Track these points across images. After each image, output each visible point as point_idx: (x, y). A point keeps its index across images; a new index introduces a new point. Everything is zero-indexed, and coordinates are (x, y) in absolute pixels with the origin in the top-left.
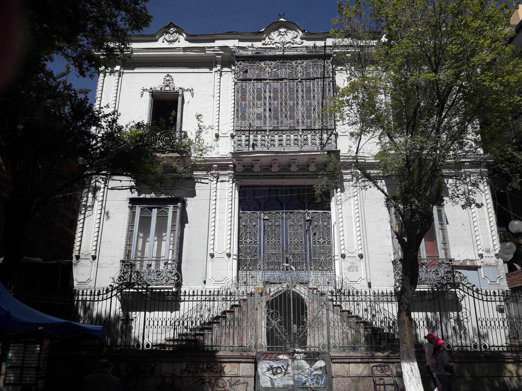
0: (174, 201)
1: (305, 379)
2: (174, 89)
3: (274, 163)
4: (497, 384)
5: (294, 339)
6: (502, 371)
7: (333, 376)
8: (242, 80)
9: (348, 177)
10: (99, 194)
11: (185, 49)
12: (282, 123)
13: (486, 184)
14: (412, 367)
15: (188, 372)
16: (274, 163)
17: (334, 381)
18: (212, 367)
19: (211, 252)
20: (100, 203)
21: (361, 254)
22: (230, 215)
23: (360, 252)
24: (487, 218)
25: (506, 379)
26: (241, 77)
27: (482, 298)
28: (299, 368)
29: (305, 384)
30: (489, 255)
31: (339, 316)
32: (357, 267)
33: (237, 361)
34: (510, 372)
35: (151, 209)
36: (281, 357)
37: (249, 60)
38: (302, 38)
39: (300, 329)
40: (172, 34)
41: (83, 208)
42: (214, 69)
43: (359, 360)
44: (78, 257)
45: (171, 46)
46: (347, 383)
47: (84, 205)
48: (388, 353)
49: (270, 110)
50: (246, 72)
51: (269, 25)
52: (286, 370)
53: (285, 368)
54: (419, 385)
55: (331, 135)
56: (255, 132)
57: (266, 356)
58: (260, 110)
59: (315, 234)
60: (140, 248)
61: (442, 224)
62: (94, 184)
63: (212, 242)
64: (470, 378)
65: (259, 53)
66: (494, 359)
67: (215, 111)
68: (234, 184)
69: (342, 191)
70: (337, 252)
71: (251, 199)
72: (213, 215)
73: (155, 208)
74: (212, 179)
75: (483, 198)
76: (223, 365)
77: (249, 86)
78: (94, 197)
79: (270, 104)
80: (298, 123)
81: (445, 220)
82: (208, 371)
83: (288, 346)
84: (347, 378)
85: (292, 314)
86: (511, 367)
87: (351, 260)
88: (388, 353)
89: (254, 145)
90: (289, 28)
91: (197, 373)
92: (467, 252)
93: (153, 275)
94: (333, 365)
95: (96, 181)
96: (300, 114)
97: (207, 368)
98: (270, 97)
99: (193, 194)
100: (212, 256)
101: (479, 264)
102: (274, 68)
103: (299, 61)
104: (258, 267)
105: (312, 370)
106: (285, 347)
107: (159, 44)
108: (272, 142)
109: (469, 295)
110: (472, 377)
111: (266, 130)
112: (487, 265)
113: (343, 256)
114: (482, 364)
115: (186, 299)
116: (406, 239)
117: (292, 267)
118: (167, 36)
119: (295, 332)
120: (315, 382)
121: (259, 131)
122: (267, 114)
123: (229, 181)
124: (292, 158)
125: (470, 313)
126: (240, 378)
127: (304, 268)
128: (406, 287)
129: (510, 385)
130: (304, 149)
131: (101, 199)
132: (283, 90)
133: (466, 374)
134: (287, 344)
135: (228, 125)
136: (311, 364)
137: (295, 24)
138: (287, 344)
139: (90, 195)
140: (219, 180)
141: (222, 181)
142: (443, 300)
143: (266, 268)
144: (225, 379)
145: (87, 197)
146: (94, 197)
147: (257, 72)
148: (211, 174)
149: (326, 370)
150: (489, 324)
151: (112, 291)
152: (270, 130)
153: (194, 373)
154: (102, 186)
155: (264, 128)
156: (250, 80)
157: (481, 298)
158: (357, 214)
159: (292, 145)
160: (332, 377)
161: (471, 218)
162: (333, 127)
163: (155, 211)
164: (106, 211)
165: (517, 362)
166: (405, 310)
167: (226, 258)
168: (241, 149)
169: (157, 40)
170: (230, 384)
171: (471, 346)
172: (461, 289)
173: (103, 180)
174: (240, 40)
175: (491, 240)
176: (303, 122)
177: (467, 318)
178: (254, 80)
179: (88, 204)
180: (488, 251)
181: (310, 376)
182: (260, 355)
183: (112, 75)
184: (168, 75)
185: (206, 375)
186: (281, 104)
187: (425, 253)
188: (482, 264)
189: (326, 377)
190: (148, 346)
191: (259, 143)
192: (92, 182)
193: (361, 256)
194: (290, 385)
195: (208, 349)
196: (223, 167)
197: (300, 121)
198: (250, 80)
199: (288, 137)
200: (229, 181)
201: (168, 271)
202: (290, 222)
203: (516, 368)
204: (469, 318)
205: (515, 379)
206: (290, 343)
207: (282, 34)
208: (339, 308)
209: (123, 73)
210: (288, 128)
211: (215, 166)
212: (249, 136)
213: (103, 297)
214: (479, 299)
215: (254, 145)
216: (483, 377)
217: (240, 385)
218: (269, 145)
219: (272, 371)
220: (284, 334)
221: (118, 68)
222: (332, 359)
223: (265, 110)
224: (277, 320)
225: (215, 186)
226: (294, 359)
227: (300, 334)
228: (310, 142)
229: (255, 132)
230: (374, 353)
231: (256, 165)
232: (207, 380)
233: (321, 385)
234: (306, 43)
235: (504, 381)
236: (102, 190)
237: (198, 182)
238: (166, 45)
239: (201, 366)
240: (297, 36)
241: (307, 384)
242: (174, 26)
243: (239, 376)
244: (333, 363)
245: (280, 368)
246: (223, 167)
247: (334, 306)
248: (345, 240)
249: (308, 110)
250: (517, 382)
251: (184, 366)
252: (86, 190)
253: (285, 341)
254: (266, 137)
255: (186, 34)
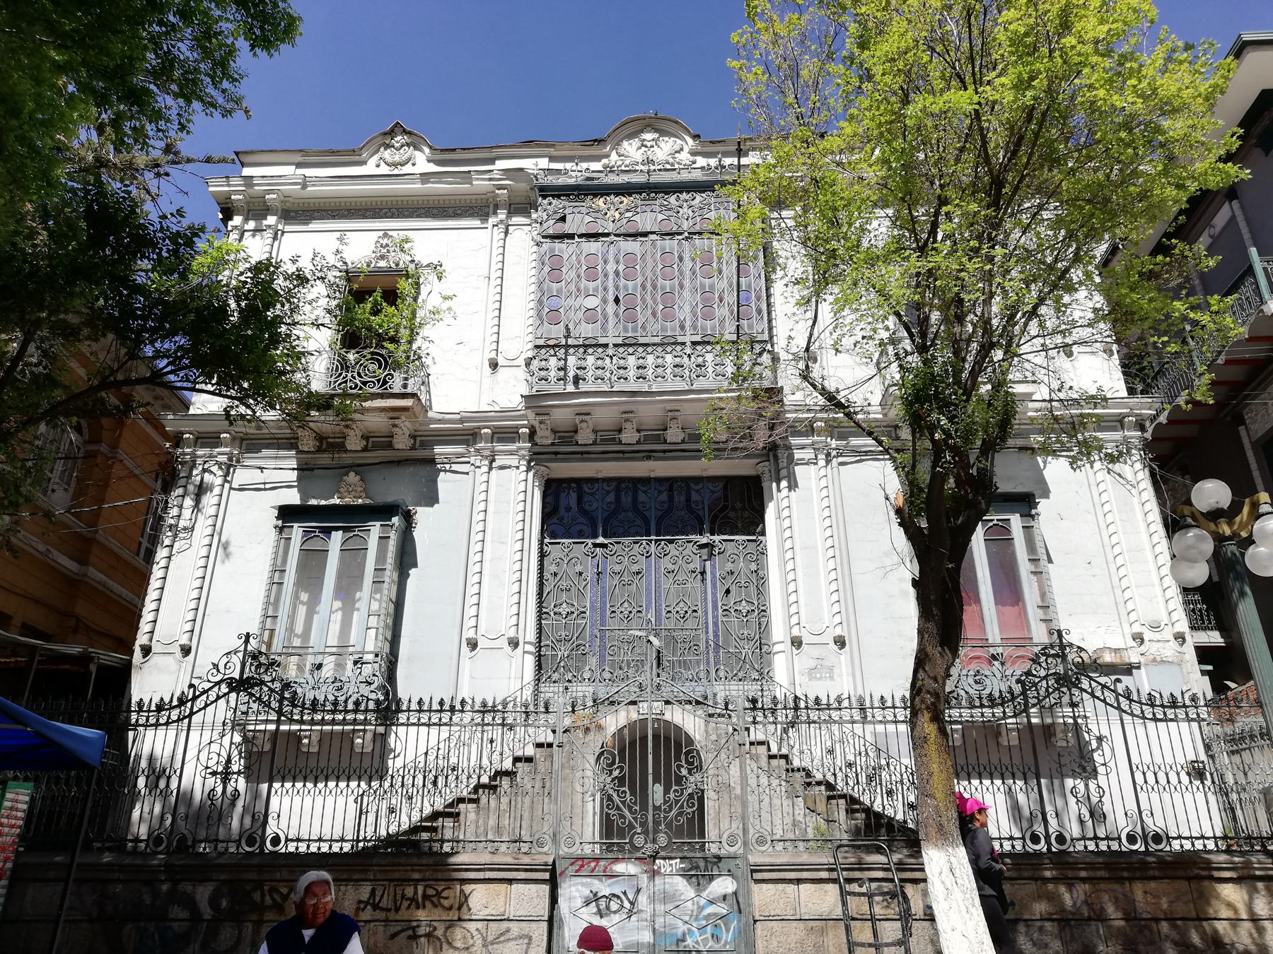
0: (383, 512)
1: (682, 928)
2: (397, 265)
3: (627, 420)
4: (1196, 939)
5: (657, 823)
6: (1208, 903)
7: (757, 918)
8: (554, 237)
9: (807, 454)
10: (209, 500)
11: (425, 177)
12: (643, 327)
13: (1138, 466)
14: (953, 859)
15: (376, 907)
16: (627, 420)
17: (758, 932)
18: (438, 894)
19: (471, 634)
20: (210, 521)
21: (840, 636)
22: (518, 546)
23: (838, 631)
24: (1148, 547)
25: (1221, 926)
26: (551, 231)
27: (1142, 712)
28: (666, 897)
29: (684, 940)
30: (1157, 636)
31: (783, 783)
32: (831, 669)
33: (504, 876)
34: (1230, 905)
35: (327, 531)
36: (620, 868)
37: (568, 195)
38: (694, 153)
39: (672, 796)
40: (398, 149)
41: (169, 534)
42: (492, 220)
43: (824, 875)
44: (147, 651)
45: (396, 172)
46: (793, 938)
47: (171, 526)
48: (900, 856)
49: (617, 300)
50: (563, 219)
51: (617, 124)
52: (632, 903)
53: (631, 897)
54: (973, 910)
55: (760, 354)
56: (581, 350)
57: (582, 866)
58: (592, 302)
59: (728, 592)
60: (299, 629)
61: (1034, 561)
62: (199, 478)
63: (473, 611)
64: (1122, 923)
65: (592, 179)
66: (1188, 871)
67: (490, 310)
68: (531, 474)
69: (793, 485)
70: (779, 632)
71: (570, 510)
72: (478, 547)
73: (337, 529)
74: (478, 464)
75: (1136, 500)
76: (468, 888)
77: (565, 249)
78: (197, 506)
79: (617, 288)
80: (682, 327)
81: (1041, 551)
82: (428, 904)
83: (639, 840)
84: (794, 924)
85: (650, 757)
86: (1231, 893)
87: (815, 651)
88: (900, 856)
89: (576, 380)
90: (663, 133)
91: (397, 909)
92: (1102, 630)
93: (324, 689)
94: (756, 888)
95: (204, 471)
96: (687, 308)
97: (425, 897)
98: (617, 273)
99: (431, 498)
100: (473, 645)
101: (1134, 659)
102: (628, 211)
103: (684, 196)
104: (586, 675)
105: (703, 902)
106: (631, 842)
107: (370, 168)
108: (622, 371)
109: (1107, 704)
110: (1126, 919)
111: (606, 346)
112: (1154, 660)
113: (797, 643)
114: (1153, 884)
115: (444, 720)
116: (924, 525)
117: (652, 638)
118: (387, 154)
119: (658, 804)
120: (709, 935)
121: (591, 346)
122: (611, 308)
123: (518, 468)
124: (669, 407)
125: (1113, 750)
126: (511, 925)
127: (702, 675)
128: (929, 649)
129: (1233, 944)
130: (699, 384)
131: (212, 511)
132: (648, 257)
133: (1111, 910)
134: (635, 833)
135: (519, 337)
136: (699, 887)
137: (676, 122)
138: (635, 833)
139: (188, 502)
140: (494, 465)
141: (502, 468)
142: (1053, 754)
143: (607, 675)
144: (472, 926)
145: (181, 507)
146: (197, 506)
147: (587, 219)
148: (477, 450)
149: (737, 901)
150: (1163, 781)
151: (195, 698)
152: (615, 345)
153: (389, 910)
154: (219, 481)
155: (602, 341)
156: (571, 236)
157: (1137, 712)
158: (830, 541)
159: (669, 376)
160: (755, 921)
161: (1108, 549)
162: (766, 337)
163: (337, 537)
164: (223, 540)
165: (1245, 878)
166: (927, 708)
167: (508, 649)
168: (546, 388)
169: (364, 163)
170: (484, 939)
171: (1119, 838)
172: (1085, 691)
173: (220, 468)
174: (552, 159)
175: (1161, 600)
176: (694, 327)
177: (1105, 764)
178: (581, 236)
179: (182, 524)
180: (1155, 627)
181: (697, 919)
182: (566, 863)
183: (258, 237)
184: (385, 235)
185: (421, 915)
186: (644, 287)
187: (997, 630)
188: (1142, 660)
189: (739, 921)
190: (276, 841)
191: (590, 374)
192: (195, 472)
193: (841, 642)
194: (643, 944)
195: (430, 848)
196: (505, 435)
197: (688, 324)
198: (571, 236)
199: (660, 360)
200: (518, 468)
201: (361, 679)
202: (666, 563)
203: (1246, 897)
204: (1112, 764)
205: (1248, 925)
206: (646, 832)
207: (649, 144)
208: (783, 762)
209: (283, 233)
210: (657, 340)
211: (486, 430)
212: (566, 360)
213: (169, 717)
214: (1132, 715)
215: (576, 380)
216: (1157, 920)
217: (511, 944)
218: (614, 378)
219: (598, 906)
220: (630, 809)
221: (271, 220)
222: (753, 871)
223: (605, 301)
224: (611, 772)
225: (485, 477)
226: (654, 874)
227: (671, 810)
228: (710, 370)
229: (581, 350)
230: (863, 855)
231: (584, 425)
232: (422, 931)
233: (726, 943)
234: (701, 161)
235: (1216, 931)
236: (217, 491)
237: (445, 471)
238: (384, 170)
239: (409, 891)
240: (682, 149)
241: (689, 942)
242: (405, 132)
243: (508, 920)
244: (757, 881)
245: (618, 897)
246: (505, 435)
247: (771, 757)
248: (801, 602)
249: (708, 305)
250: (1251, 935)
251: (365, 891)
252: (180, 491)
253: (631, 826)
254: (608, 360)
255: (430, 147)
